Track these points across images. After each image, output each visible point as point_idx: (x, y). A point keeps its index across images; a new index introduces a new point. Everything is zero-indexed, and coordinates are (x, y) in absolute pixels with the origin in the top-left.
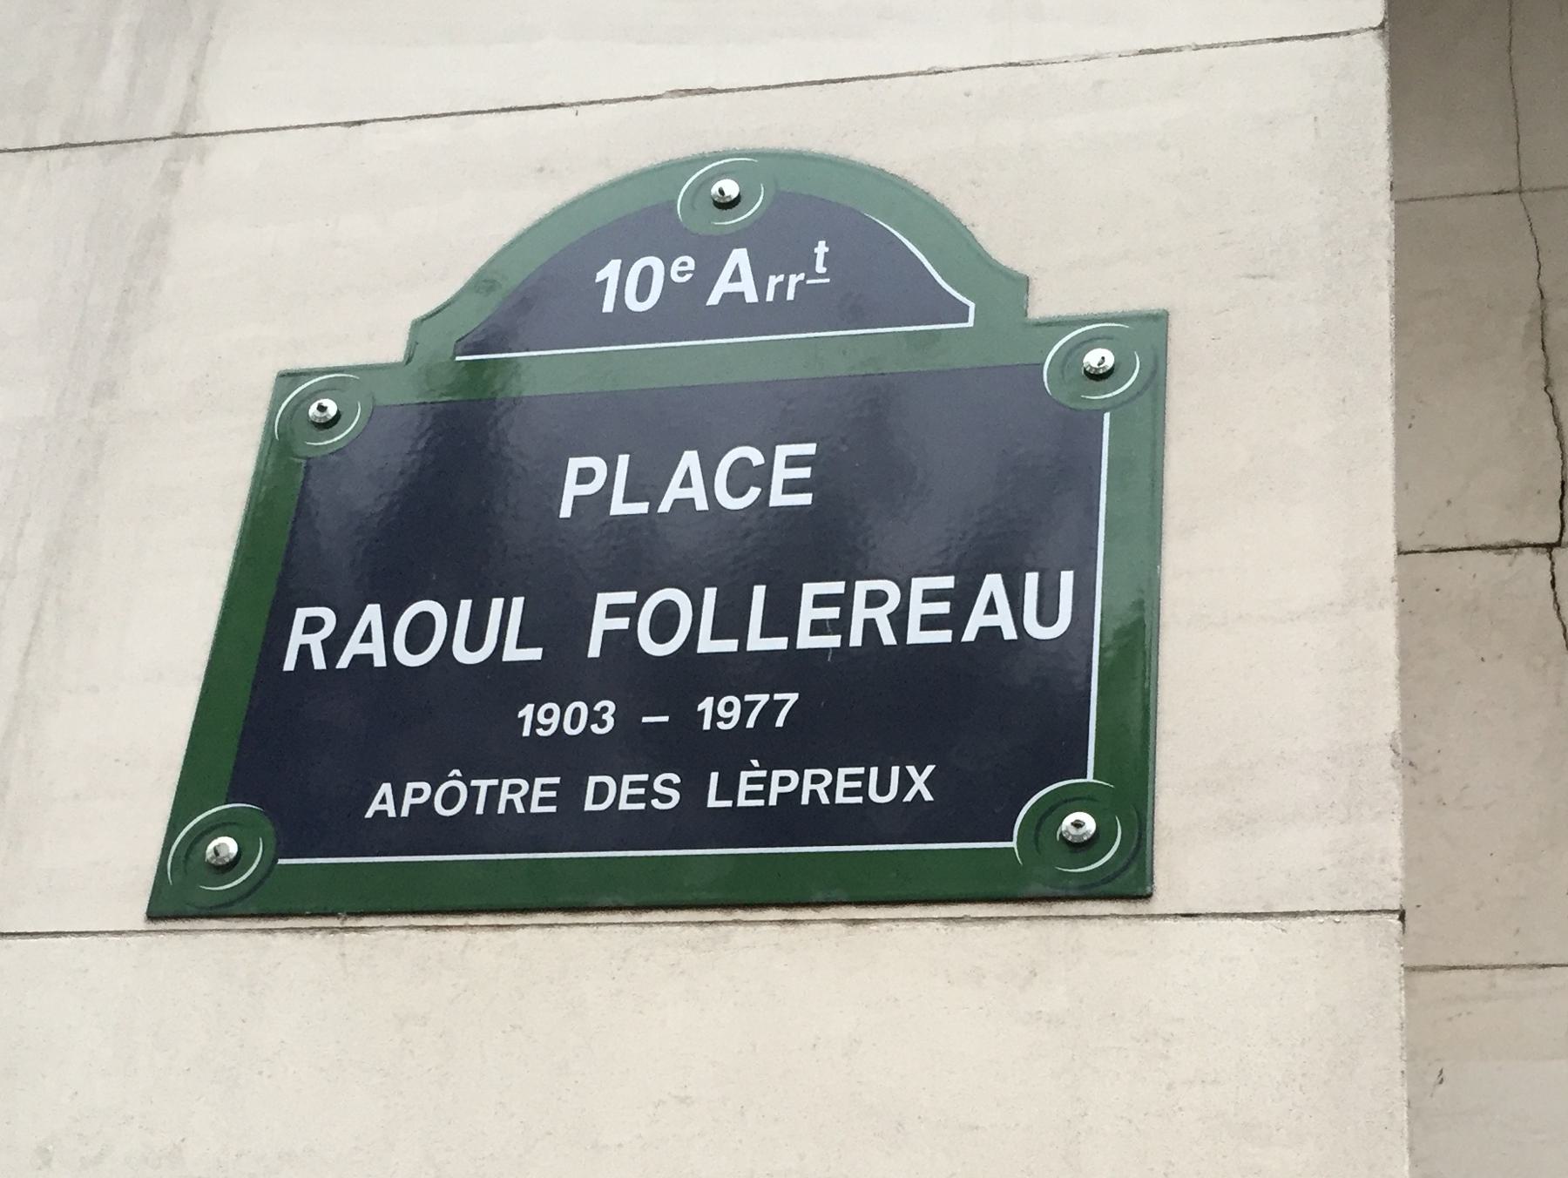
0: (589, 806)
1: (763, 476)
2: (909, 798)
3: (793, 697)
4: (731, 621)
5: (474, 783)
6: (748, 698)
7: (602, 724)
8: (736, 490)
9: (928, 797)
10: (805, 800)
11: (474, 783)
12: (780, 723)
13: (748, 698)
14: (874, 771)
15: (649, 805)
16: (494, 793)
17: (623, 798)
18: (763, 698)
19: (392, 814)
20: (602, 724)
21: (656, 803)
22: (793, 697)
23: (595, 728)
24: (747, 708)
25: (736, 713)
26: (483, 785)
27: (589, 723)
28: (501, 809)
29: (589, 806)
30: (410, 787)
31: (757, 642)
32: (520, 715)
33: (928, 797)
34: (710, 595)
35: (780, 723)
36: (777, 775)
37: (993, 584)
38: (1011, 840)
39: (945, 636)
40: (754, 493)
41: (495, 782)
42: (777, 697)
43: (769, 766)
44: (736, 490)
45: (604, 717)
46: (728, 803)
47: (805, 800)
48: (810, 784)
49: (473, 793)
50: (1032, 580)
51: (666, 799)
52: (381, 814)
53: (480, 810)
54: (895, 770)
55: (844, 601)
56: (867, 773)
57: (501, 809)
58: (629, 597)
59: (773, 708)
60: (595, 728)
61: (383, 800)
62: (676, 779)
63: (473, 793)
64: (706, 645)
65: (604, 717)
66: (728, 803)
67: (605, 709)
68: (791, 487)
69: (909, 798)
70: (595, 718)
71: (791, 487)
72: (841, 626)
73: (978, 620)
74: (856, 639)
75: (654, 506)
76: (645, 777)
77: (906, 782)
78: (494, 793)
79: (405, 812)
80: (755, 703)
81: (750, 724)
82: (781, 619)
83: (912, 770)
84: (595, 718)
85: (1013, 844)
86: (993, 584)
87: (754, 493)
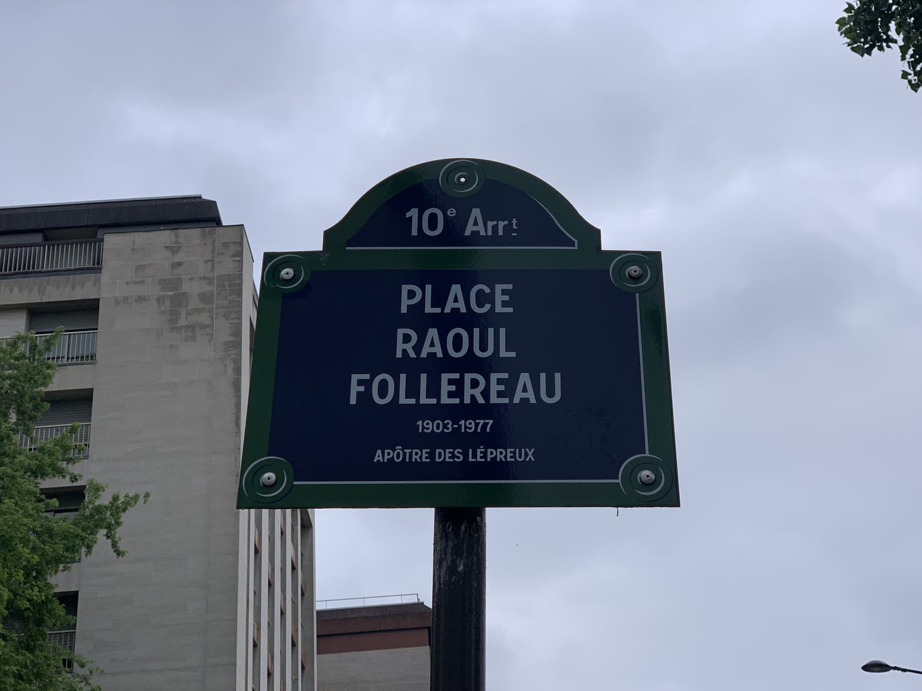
0: (437, 460)
1: (491, 298)
2: (527, 460)
3: (491, 422)
4: (413, 391)
5: (405, 451)
6: (477, 421)
7: (448, 429)
8: (480, 305)
9: (533, 460)
10: (498, 460)
11: (405, 451)
12: (488, 430)
13: (477, 421)
14: (517, 450)
15: (454, 460)
16: (411, 454)
17: (447, 458)
18: (482, 422)
19: (382, 461)
20: (448, 429)
21: (456, 459)
22: (491, 422)
23: (445, 430)
24: (477, 425)
25: (473, 426)
26: (408, 451)
27: (443, 429)
28: (414, 460)
29: (437, 460)
30: (386, 451)
31: (424, 400)
32: (418, 423)
33: (533, 460)
34: (403, 377)
35: (488, 430)
36: (489, 451)
37: (525, 378)
38: (617, 478)
39: (506, 401)
40: (488, 307)
41: (410, 451)
42: (486, 421)
43: (486, 448)
44: (480, 305)
45: (448, 426)
46: (475, 460)
47: (498, 460)
48: (500, 454)
49: (405, 454)
50: (543, 376)
51: (459, 458)
52: (378, 461)
53: (407, 460)
54: (523, 450)
55: (459, 383)
56: (515, 451)
57: (414, 460)
58: (367, 376)
59: (485, 425)
60: (445, 430)
61: (378, 457)
62: (461, 451)
63: (405, 454)
64: (403, 400)
65: (448, 426)
66: (475, 460)
67: (448, 423)
68: (504, 304)
69: (527, 460)
70: (445, 426)
71: (504, 304)
72: (459, 393)
73: (518, 396)
74: (467, 400)
75: (443, 310)
76: (452, 450)
77: (526, 455)
78: (411, 454)
79: (386, 461)
80: (479, 423)
81: (479, 430)
82: (433, 390)
83: (527, 450)
84: (445, 426)
85: (619, 481)
86: (525, 378)
87: (488, 307)
